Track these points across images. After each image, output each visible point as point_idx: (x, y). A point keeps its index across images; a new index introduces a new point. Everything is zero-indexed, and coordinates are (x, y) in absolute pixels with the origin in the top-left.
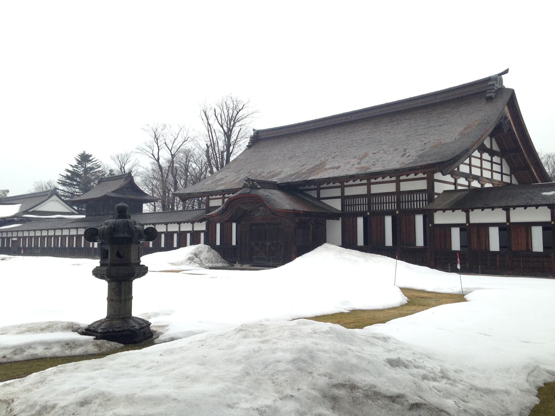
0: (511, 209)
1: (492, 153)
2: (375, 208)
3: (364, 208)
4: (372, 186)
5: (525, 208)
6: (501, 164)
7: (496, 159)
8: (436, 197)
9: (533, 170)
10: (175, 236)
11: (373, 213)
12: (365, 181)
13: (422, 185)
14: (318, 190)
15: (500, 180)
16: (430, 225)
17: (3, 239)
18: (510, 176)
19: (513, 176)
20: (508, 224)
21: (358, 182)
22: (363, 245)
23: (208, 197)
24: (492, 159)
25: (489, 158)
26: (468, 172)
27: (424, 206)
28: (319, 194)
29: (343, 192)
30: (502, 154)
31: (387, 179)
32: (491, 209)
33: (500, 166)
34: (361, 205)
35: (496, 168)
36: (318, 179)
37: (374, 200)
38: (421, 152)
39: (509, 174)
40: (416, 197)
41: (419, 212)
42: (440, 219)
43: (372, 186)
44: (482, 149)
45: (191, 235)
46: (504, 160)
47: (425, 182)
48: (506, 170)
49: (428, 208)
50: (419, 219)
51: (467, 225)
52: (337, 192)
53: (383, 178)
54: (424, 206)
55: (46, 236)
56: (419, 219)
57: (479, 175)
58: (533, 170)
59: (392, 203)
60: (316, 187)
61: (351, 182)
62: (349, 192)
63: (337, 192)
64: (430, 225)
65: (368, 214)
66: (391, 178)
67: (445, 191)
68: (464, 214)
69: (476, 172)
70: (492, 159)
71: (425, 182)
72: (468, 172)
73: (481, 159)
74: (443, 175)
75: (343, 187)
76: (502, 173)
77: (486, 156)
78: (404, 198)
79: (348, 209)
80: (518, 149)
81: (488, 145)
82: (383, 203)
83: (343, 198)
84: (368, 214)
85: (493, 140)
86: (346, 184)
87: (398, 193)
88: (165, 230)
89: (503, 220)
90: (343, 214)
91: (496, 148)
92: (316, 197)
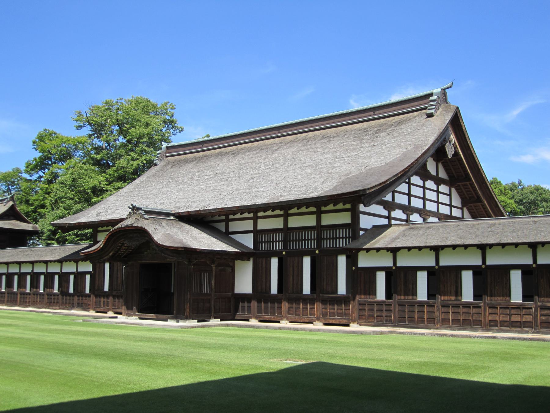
0: (488, 248)
1: (438, 181)
2: (293, 246)
3: (312, 245)
4: (259, 221)
5: (367, 252)
6: (450, 195)
7: (443, 188)
8: (361, 233)
9: (485, 202)
10: (56, 277)
11: (291, 254)
12: (251, 215)
13: (345, 218)
14: (227, 221)
15: (449, 214)
16: (354, 268)
17: (10, 277)
18: (462, 209)
19: (465, 209)
20: (534, 266)
21: (304, 209)
22: (309, 293)
23: (227, 215)
24: (438, 188)
25: (434, 187)
26: (406, 203)
27: (344, 245)
28: (227, 227)
29: (255, 225)
30: (451, 182)
31: (340, 206)
32: (463, 248)
33: (448, 197)
34: (308, 240)
35: (444, 199)
36: (244, 206)
37: (326, 234)
38: (344, 178)
39: (461, 206)
40: (339, 233)
41: (342, 251)
42: (364, 261)
43: (259, 221)
44: (425, 175)
45: (75, 277)
46: (453, 190)
47: (348, 214)
48: (456, 201)
49: (348, 247)
50: (342, 260)
51: (437, 267)
52: (248, 225)
53: (334, 206)
54: (344, 245)
55: (4, 274)
56: (342, 260)
57: (422, 207)
58: (485, 202)
59: (279, 241)
60: (282, 212)
61: (238, 216)
62: (263, 225)
63: (248, 225)
64: (354, 268)
65: (284, 253)
66: (344, 205)
67: (374, 226)
68: (75, 264)
69: (417, 203)
70: (438, 188)
71: (348, 214)
72: (406, 203)
73: (424, 188)
74: (365, 206)
75: (255, 219)
76: (451, 206)
77: (430, 184)
78: (293, 236)
79: (262, 247)
80: (468, 178)
81: (433, 172)
82: (270, 242)
83: (256, 232)
84: (284, 253)
85: (440, 166)
86: (323, 209)
87: (319, 228)
88: (44, 271)
89: (432, 263)
90: (255, 253)
91: (443, 174)
92: (224, 231)
